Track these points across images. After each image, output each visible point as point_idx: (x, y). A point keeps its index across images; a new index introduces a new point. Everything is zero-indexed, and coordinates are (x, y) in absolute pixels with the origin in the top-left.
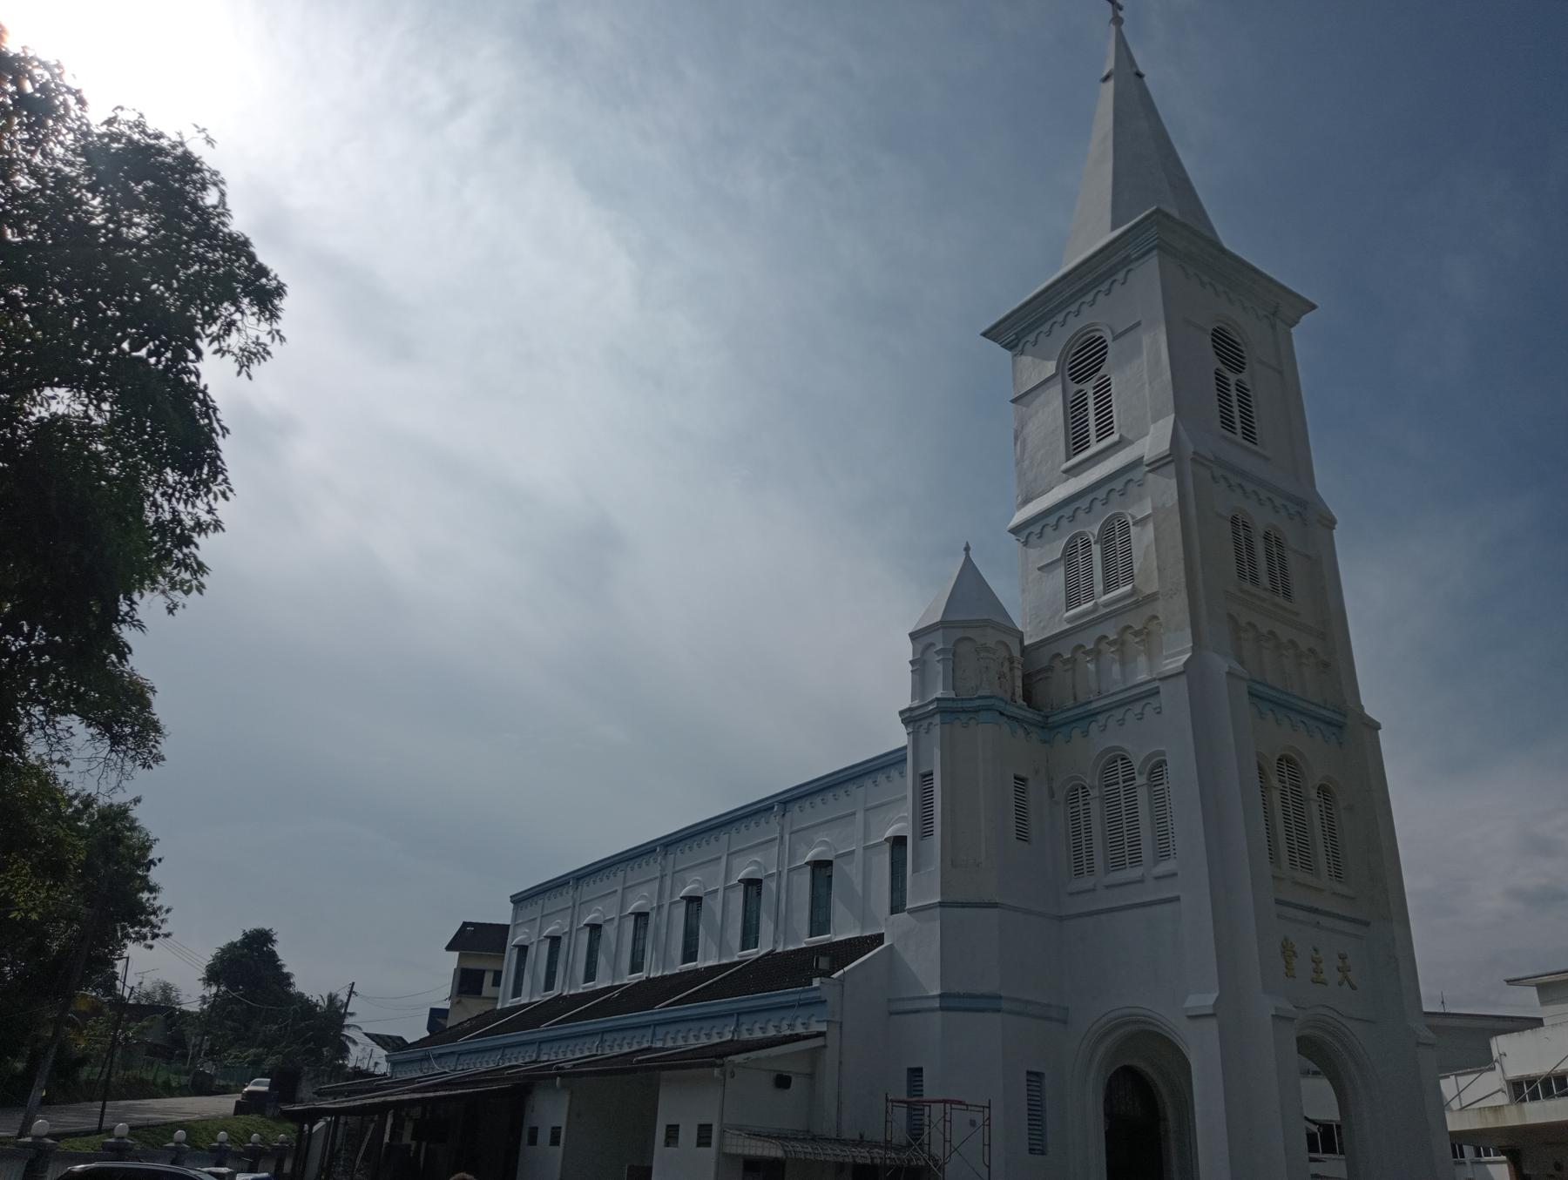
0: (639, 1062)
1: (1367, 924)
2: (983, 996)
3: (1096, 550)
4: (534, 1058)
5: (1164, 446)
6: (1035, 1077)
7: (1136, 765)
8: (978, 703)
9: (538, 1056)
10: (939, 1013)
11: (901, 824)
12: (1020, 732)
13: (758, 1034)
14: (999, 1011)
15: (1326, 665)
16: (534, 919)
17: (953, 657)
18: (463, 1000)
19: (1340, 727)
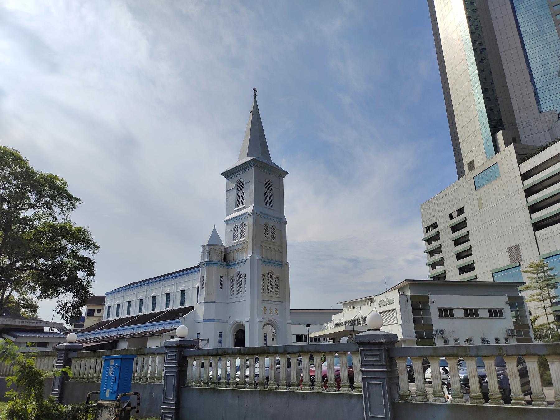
0: (143, 335)
1: (282, 302)
2: (211, 319)
3: (239, 229)
4: (117, 334)
5: (251, 212)
6: (220, 333)
7: (242, 275)
8: (214, 262)
9: (118, 333)
10: (203, 323)
11: (198, 284)
12: (222, 267)
13: (168, 328)
14: (214, 322)
15: (281, 252)
16: (113, 299)
17: (210, 252)
18: (89, 317)
19: (282, 265)
